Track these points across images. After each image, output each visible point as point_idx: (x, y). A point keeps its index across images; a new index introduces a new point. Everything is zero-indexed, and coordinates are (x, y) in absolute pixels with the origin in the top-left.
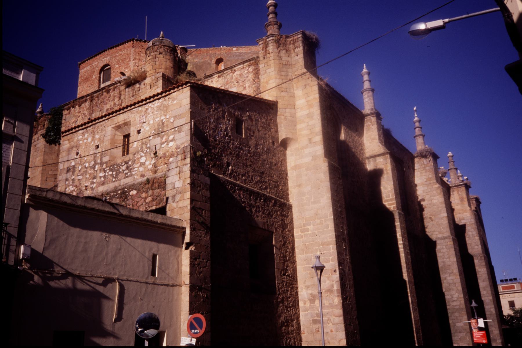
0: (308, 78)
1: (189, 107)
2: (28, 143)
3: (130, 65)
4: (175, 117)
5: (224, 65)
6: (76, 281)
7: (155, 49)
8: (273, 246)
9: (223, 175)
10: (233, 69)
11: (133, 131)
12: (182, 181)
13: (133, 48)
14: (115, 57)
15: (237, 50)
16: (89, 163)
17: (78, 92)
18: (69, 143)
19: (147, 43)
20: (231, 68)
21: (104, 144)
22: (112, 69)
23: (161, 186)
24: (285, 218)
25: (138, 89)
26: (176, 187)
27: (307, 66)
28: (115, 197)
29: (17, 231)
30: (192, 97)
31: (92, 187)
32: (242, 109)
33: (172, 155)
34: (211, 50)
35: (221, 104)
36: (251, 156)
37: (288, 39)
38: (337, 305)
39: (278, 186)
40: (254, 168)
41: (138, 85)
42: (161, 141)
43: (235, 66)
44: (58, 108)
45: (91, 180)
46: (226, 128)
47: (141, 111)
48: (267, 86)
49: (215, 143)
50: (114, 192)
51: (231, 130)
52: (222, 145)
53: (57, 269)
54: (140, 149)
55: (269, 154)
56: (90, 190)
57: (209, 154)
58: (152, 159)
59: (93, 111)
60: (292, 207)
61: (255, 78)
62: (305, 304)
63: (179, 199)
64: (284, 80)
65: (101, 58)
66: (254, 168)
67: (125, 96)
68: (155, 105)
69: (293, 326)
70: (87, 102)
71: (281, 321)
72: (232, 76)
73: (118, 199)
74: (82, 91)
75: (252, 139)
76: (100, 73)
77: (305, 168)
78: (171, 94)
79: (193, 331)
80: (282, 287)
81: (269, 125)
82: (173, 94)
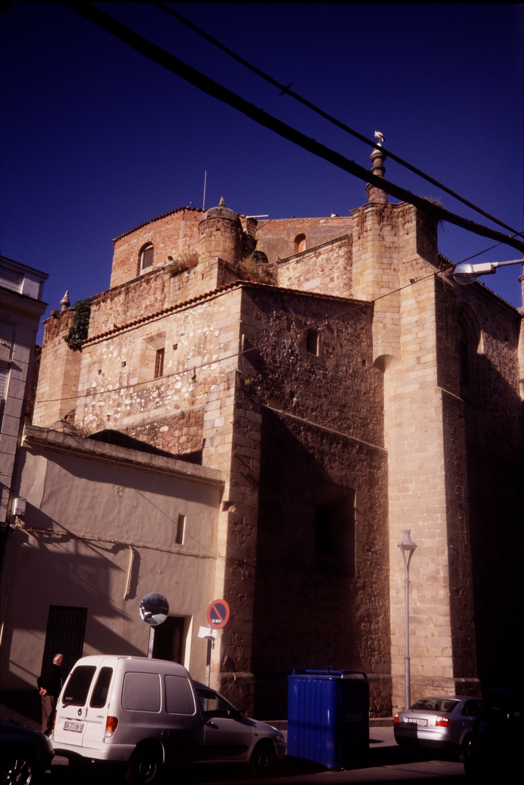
0: (421, 268)
1: (239, 317)
2: (27, 371)
3: (178, 244)
4: (221, 329)
5: (306, 245)
6: (79, 545)
7: (210, 224)
8: (354, 509)
9: (284, 410)
10: (318, 251)
11: (168, 346)
12: (223, 419)
13: (184, 220)
14: (160, 232)
15: (325, 223)
16: (113, 385)
17: (112, 279)
18: (91, 357)
19: (202, 212)
20: (314, 249)
21: (133, 361)
22: (155, 249)
23: (198, 422)
24: (375, 471)
25: (187, 280)
26: (216, 425)
27: (420, 251)
28: (142, 433)
29: (11, 480)
30: (244, 302)
31: (116, 417)
32: (318, 317)
33: (214, 382)
34: (290, 222)
35: (285, 309)
36: (327, 382)
37: (395, 210)
38: (442, 599)
39: (368, 424)
40: (332, 400)
41: (186, 274)
42: (202, 362)
43: (320, 247)
44: (85, 301)
45: (114, 409)
46: (292, 343)
47: (179, 319)
48: (360, 278)
49: (274, 366)
50: (141, 426)
51: (300, 346)
52: (284, 367)
53: (57, 529)
54: (175, 370)
55: (356, 379)
56: (114, 421)
57: (265, 381)
58: (190, 385)
59: (128, 308)
60: (387, 455)
61: (347, 265)
62: (398, 593)
63: (218, 442)
64: (385, 271)
65: (141, 234)
66: (332, 400)
67: (170, 288)
68: (198, 311)
69: (377, 622)
70: (122, 295)
71: (359, 615)
72: (316, 261)
73: (146, 436)
74: (116, 278)
75: (330, 358)
76: (140, 255)
77: (408, 400)
78: (217, 297)
79: (213, 621)
80: (364, 567)
81: (358, 337)
82: (220, 297)
